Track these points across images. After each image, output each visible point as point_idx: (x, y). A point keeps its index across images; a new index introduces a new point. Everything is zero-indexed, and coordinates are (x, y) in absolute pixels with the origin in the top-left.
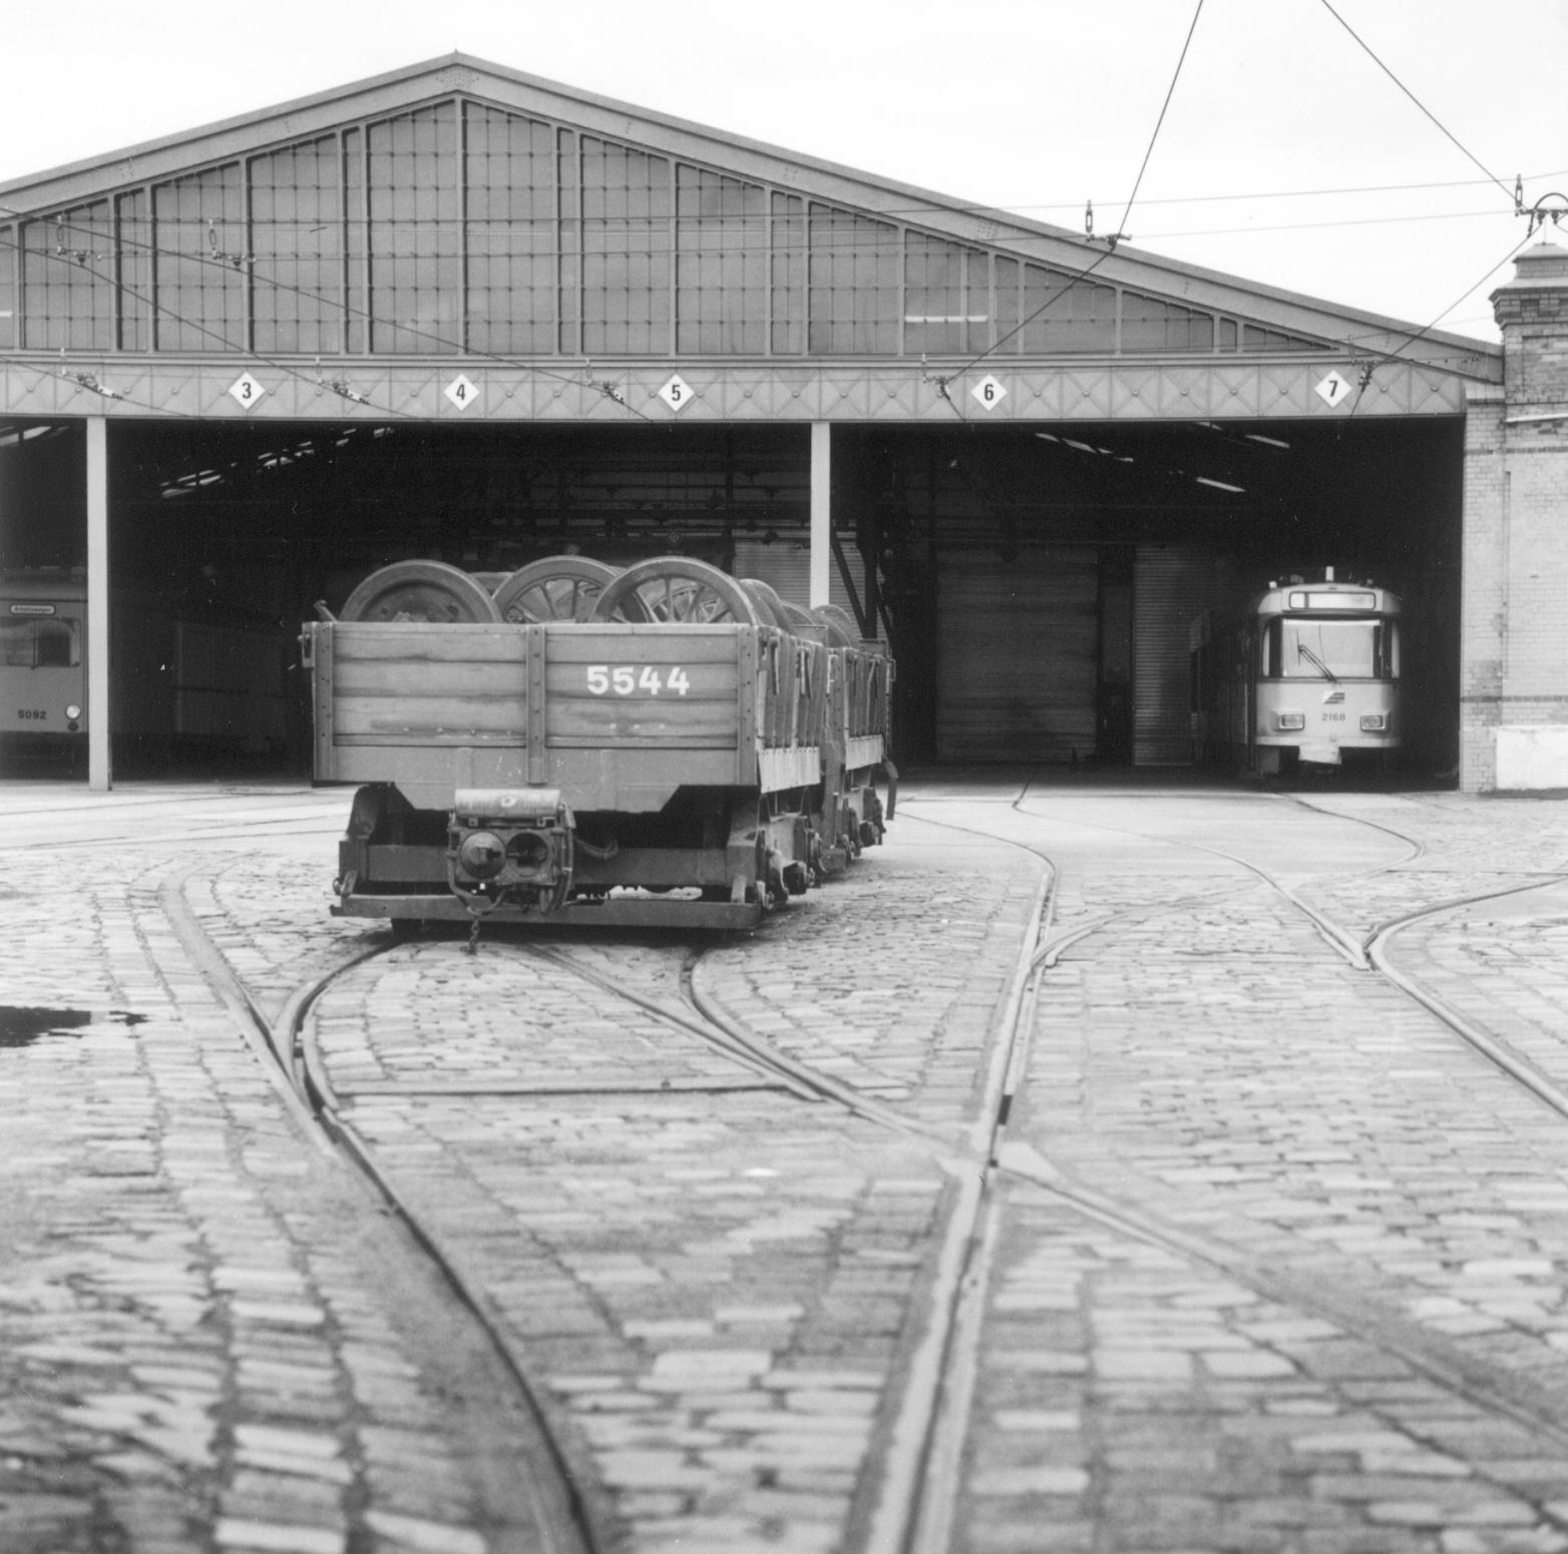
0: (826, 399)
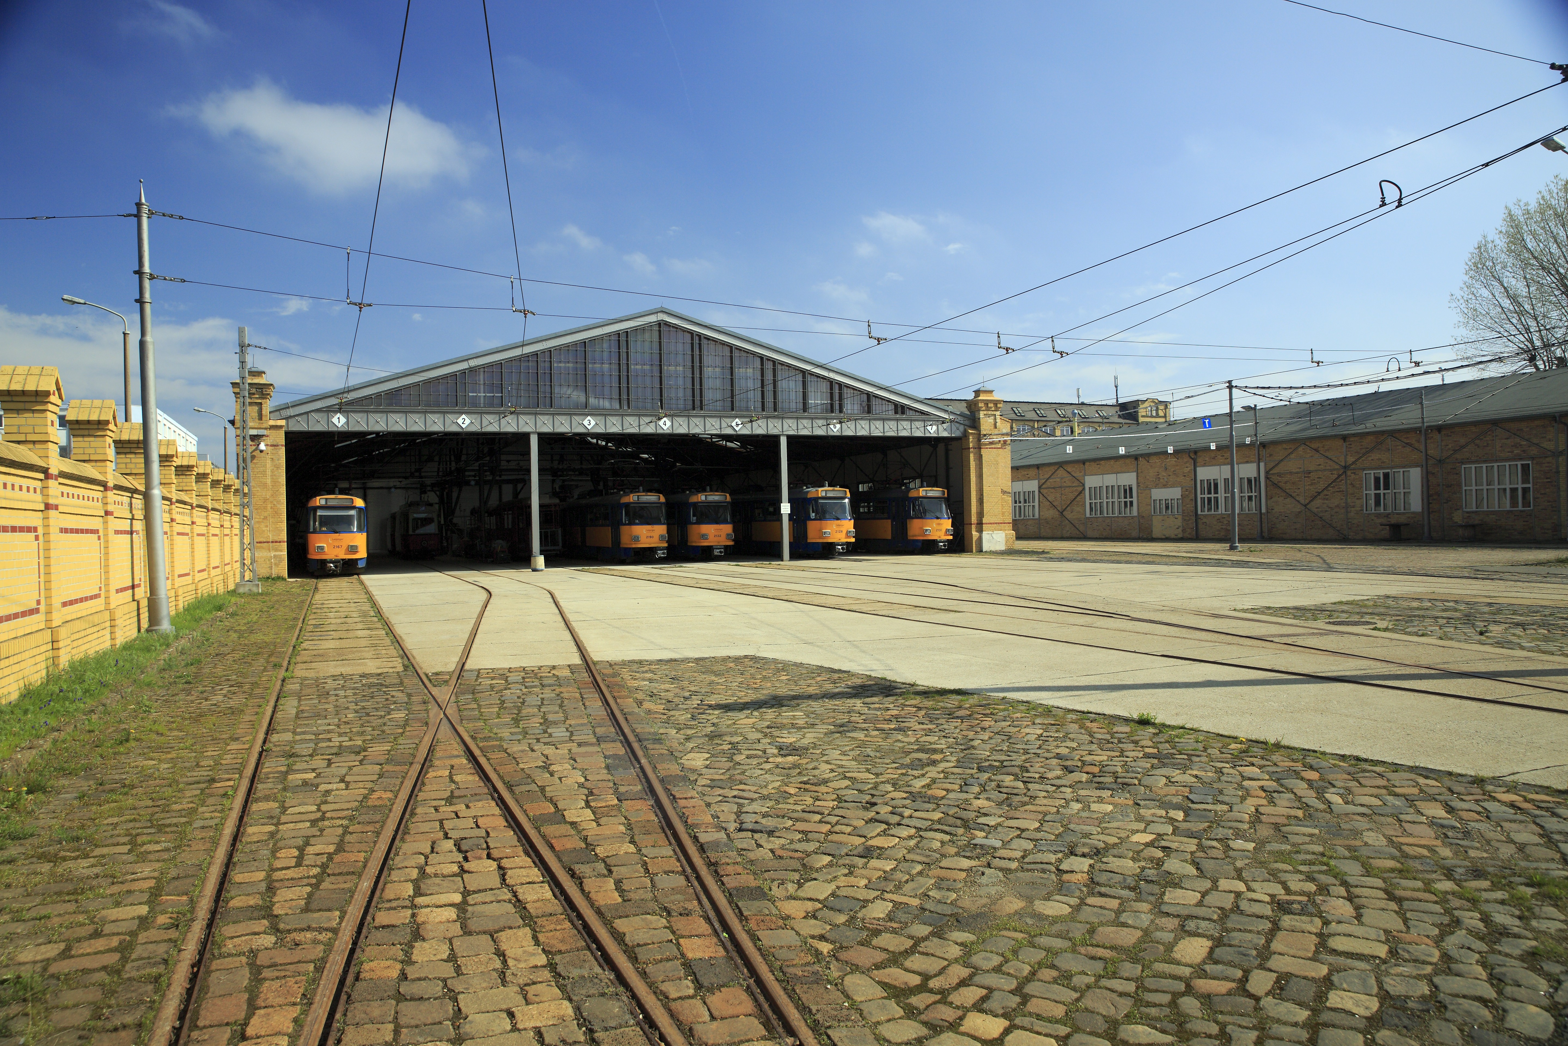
0: (534, 424)
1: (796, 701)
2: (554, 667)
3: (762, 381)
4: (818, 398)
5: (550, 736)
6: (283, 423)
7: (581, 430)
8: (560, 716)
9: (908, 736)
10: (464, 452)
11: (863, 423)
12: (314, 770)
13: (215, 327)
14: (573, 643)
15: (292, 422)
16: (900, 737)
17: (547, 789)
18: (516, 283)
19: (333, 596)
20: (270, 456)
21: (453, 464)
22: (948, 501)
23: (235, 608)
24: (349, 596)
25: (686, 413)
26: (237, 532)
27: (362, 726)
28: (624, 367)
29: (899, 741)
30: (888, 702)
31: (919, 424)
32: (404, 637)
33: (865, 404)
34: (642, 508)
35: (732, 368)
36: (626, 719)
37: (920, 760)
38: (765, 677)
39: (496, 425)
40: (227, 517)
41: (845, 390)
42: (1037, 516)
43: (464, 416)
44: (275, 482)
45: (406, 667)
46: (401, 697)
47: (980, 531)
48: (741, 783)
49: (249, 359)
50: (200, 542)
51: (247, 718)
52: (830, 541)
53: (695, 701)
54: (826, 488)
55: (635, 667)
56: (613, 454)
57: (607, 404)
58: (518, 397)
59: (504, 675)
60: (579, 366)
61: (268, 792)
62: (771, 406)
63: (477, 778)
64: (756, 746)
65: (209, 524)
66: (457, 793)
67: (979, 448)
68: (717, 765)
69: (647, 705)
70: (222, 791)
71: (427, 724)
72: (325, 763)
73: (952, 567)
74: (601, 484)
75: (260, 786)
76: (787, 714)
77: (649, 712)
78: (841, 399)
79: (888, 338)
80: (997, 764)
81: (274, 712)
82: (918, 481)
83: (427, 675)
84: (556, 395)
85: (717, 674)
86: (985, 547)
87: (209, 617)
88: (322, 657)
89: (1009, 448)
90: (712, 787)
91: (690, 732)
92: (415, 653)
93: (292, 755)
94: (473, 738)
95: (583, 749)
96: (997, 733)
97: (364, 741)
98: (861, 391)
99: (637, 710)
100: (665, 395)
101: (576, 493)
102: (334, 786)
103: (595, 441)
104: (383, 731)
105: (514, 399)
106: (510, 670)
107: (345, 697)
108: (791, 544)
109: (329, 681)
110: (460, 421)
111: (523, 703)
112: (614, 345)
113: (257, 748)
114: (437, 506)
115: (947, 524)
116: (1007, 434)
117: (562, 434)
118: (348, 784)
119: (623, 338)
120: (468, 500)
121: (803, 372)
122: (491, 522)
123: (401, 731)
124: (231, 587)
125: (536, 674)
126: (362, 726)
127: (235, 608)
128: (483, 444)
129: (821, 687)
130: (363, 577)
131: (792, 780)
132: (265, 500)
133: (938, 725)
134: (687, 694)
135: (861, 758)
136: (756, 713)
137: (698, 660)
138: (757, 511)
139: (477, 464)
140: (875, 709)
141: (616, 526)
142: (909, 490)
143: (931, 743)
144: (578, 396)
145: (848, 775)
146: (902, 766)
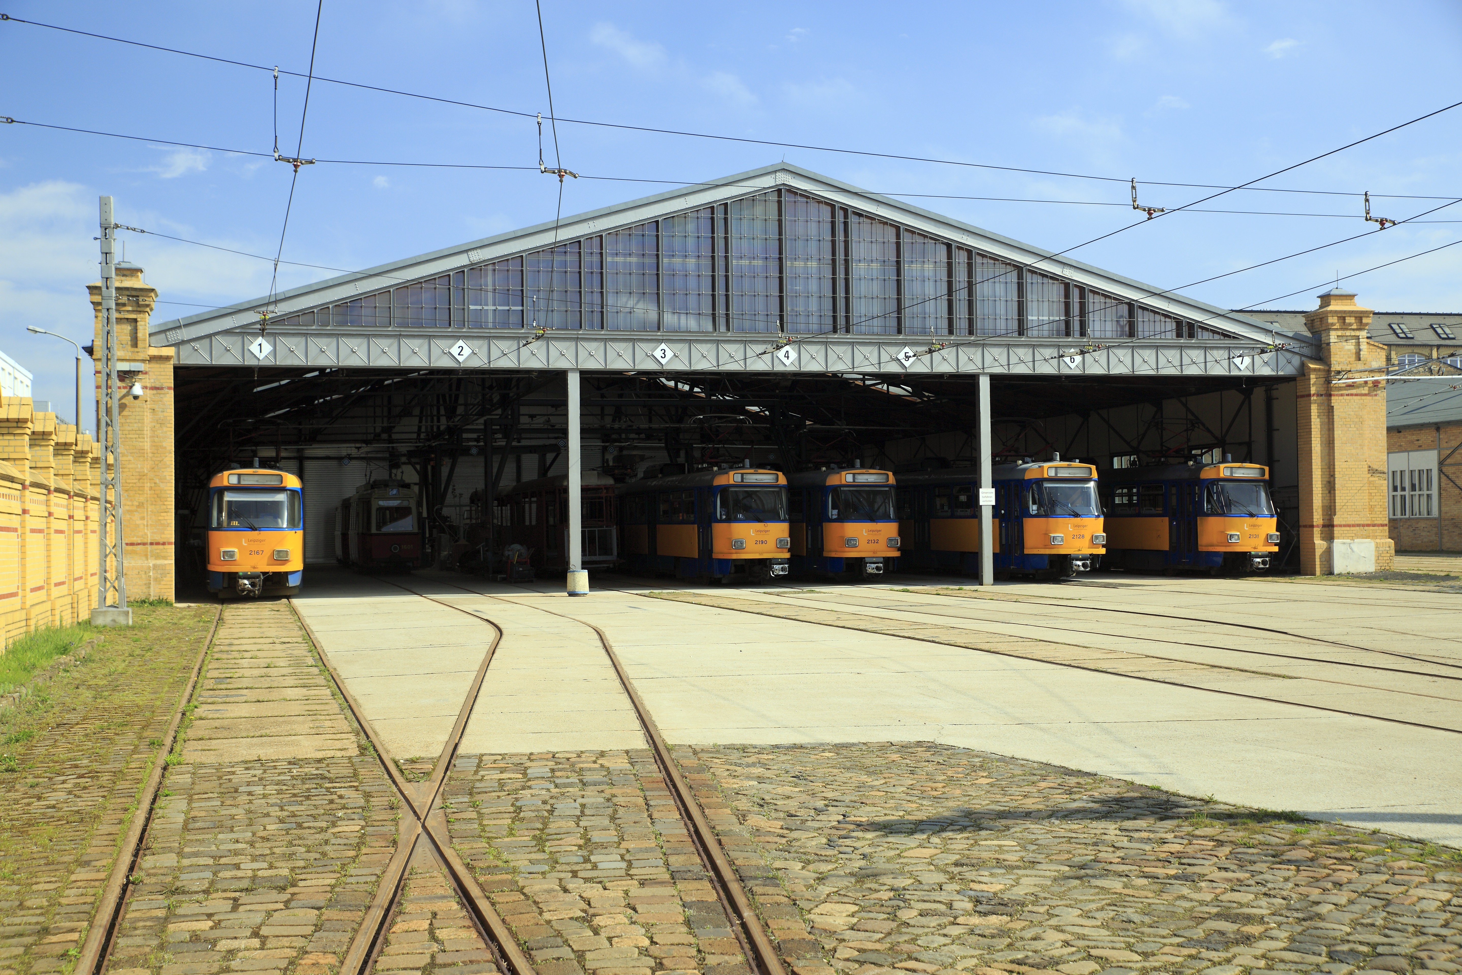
0: (573, 357)
1: (1004, 822)
2: (602, 754)
3: (950, 284)
4: (1043, 312)
5: (595, 867)
6: (171, 351)
7: (650, 366)
8: (611, 835)
9: (1200, 890)
10: (461, 400)
11: (1120, 352)
12: (210, 916)
13: (54, 197)
14: (633, 715)
15: (185, 350)
16: (1185, 891)
17: (589, 956)
18: (547, 125)
19: (247, 633)
20: (149, 405)
21: (443, 420)
22: (1271, 486)
23: (89, 650)
24: (272, 632)
25: (822, 338)
26: (95, 526)
27: (290, 844)
28: (720, 263)
29: (1183, 897)
30: (1165, 828)
31: (1220, 355)
32: (361, 700)
33: (1124, 321)
34: (749, 494)
35: (898, 263)
36: (720, 842)
37: (1222, 933)
38: (951, 779)
39: (513, 357)
40: (79, 503)
41: (1090, 298)
42: (1435, 513)
43: (461, 343)
44: (157, 448)
45: (362, 749)
46: (354, 798)
47: (1329, 537)
48: (910, 958)
49: (116, 248)
50: (35, 542)
51: (105, 829)
53: (834, 816)
54: (1057, 463)
55: (735, 756)
56: (702, 406)
57: (692, 324)
58: (550, 311)
59: (521, 765)
60: (647, 260)
61: (133, 952)
62: (963, 322)
63: (474, 935)
64: (936, 896)
65: (50, 514)
66: (440, 959)
67: (1327, 394)
68: (870, 925)
69: (755, 820)
70: (59, 950)
71: (395, 843)
72: (228, 905)
73: (1277, 600)
74: (682, 453)
75: (122, 942)
76: (988, 844)
77: (757, 832)
78: (1083, 312)
79: (1167, 207)
80: (1365, 949)
81: (148, 820)
82: (1217, 452)
83: (396, 763)
84: (609, 310)
85: (871, 772)
87: (45, 663)
88: (227, 730)
89: (1382, 394)
90: (861, 963)
91: (824, 867)
92: (378, 726)
93: (177, 891)
94: (470, 868)
95: (648, 891)
96: (1364, 894)
97: (293, 869)
98: (1119, 300)
99: (737, 828)
100: (788, 308)
101: (641, 470)
102: (242, 944)
103: (672, 384)
104: (324, 854)
105: (542, 316)
106: (530, 757)
107: (265, 796)
108: (995, 556)
109: (239, 770)
110: (455, 351)
111: (551, 812)
112: (706, 225)
113: (119, 879)
114: (416, 489)
115: (1269, 526)
116: (1380, 371)
117: (620, 372)
118: (264, 940)
119: (719, 215)
120: (467, 478)
121: (1019, 269)
122: (502, 515)
123: (352, 853)
124: (84, 616)
125: (573, 765)
126: (290, 844)
127: (89, 650)
128: (491, 387)
129: (1046, 798)
130: (296, 602)
131: (997, 956)
132: (142, 476)
133: (1253, 874)
134: (820, 804)
135: (1117, 924)
136: (935, 840)
137: (838, 748)
138: (938, 502)
139: (482, 420)
140: (1142, 840)
141: (706, 524)
142: (1200, 466)
143: (1241, 905)
144: (645, 310)
145: (1093, 952)
146: (1191, 942)
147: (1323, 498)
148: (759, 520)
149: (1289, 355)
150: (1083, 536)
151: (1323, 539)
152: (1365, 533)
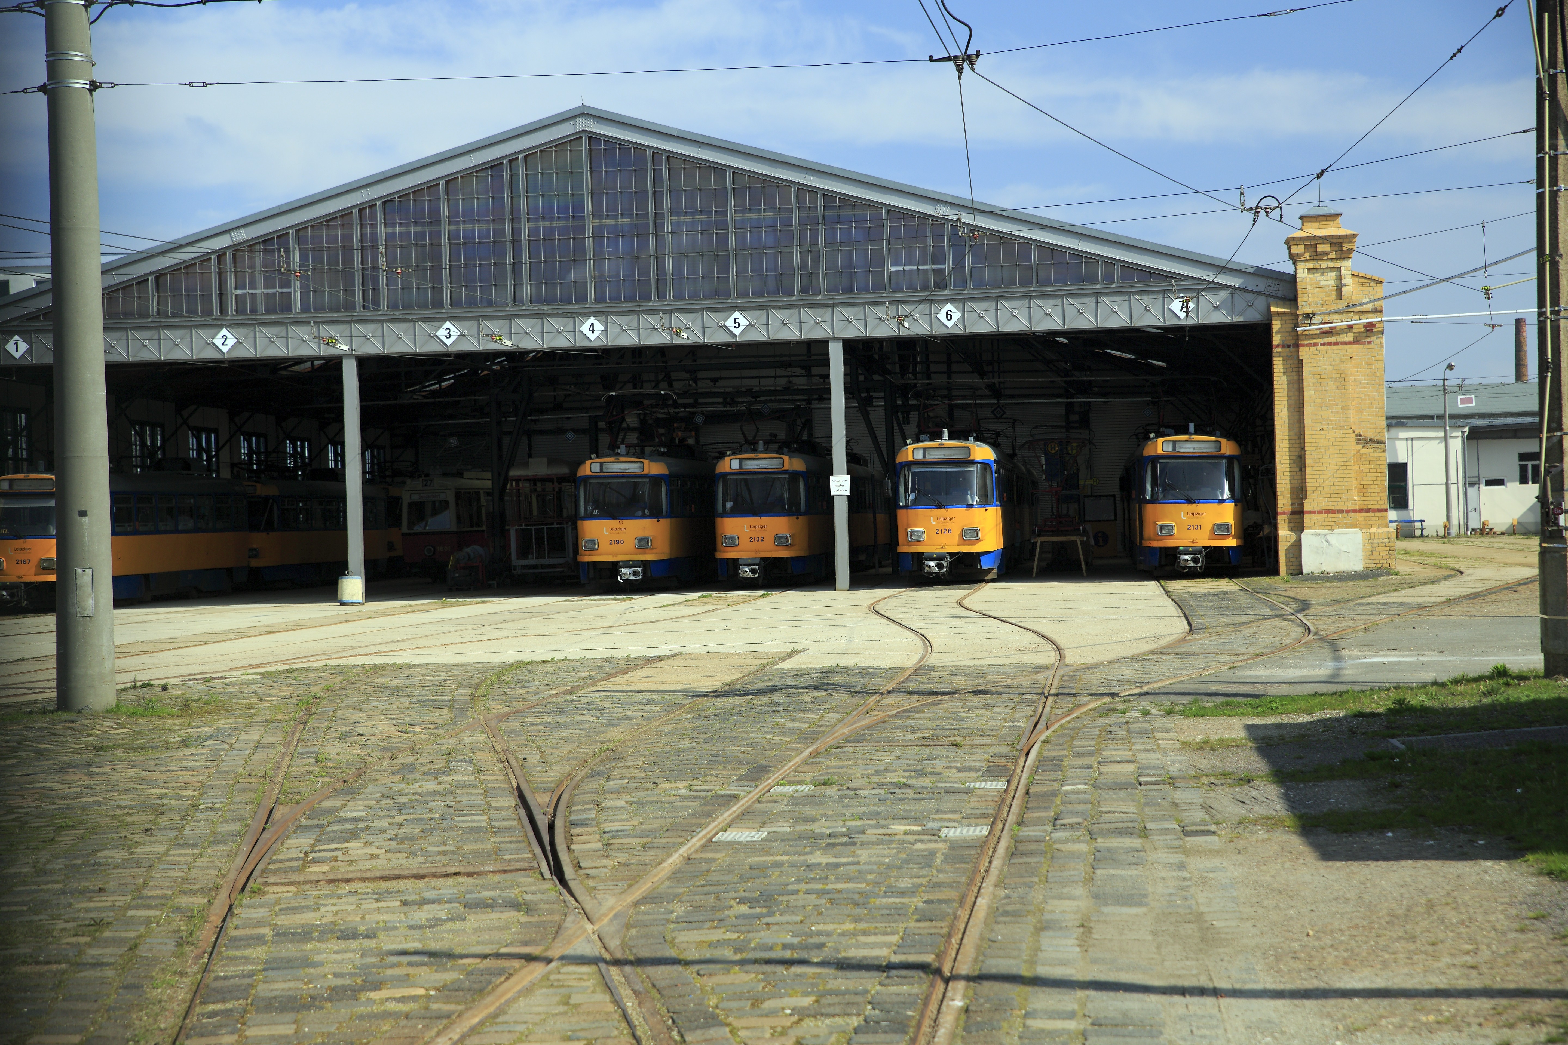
0: (348, 342)
47: (1298, 527)
52: (1171, 544)
67: (1295, 343)
86: (1308, 565)
147: (1292, 477)
148: (613, 517)
149: (1249, 297)
150: (950, 531)
151: (1291, 529)
152: (1350, 521)
